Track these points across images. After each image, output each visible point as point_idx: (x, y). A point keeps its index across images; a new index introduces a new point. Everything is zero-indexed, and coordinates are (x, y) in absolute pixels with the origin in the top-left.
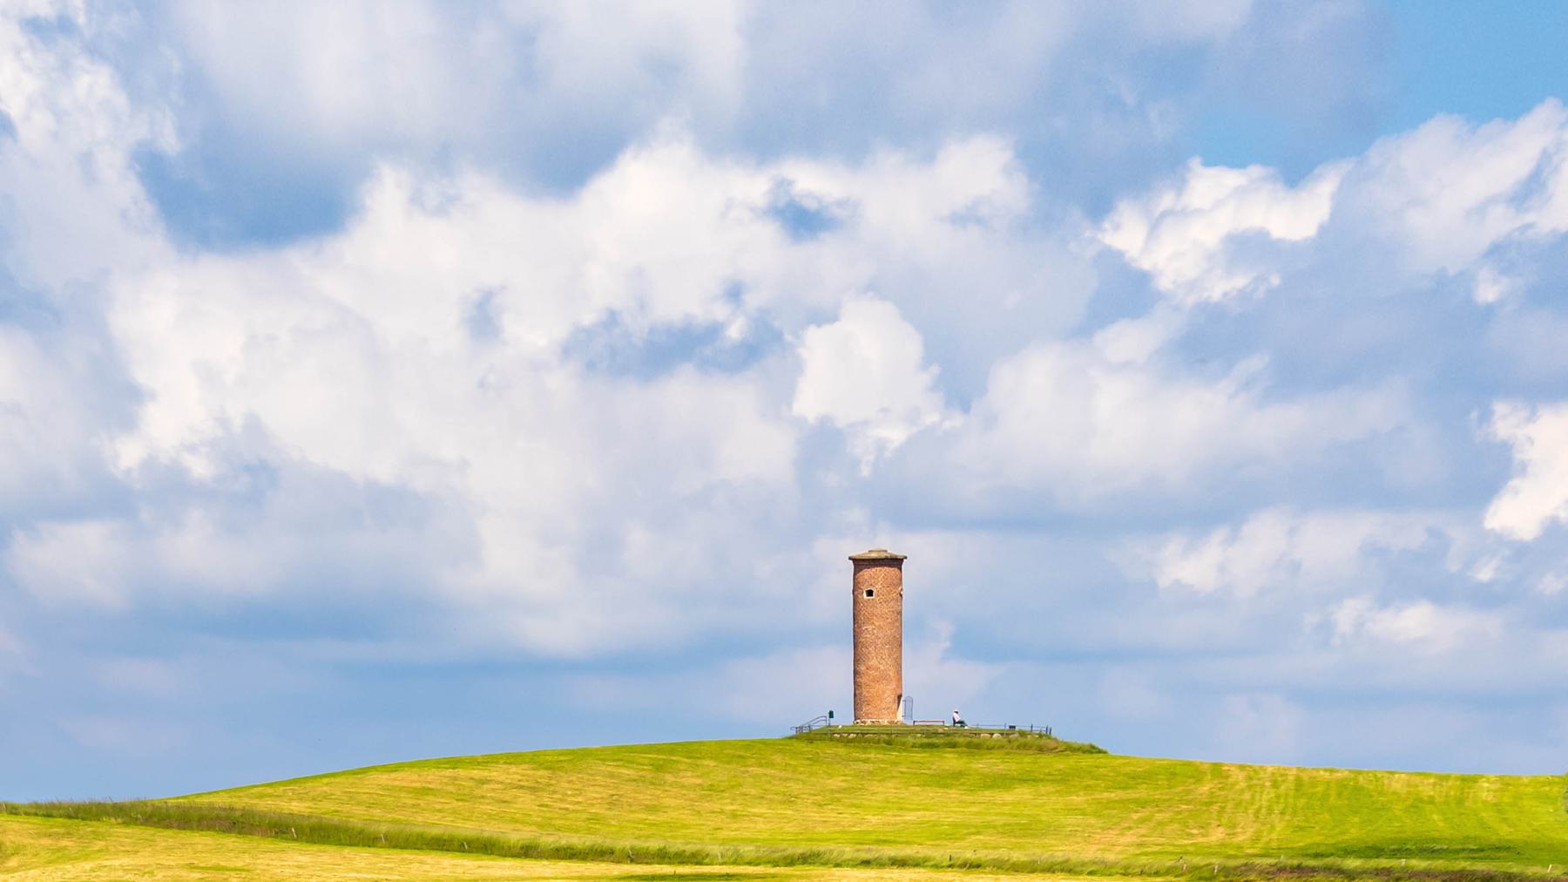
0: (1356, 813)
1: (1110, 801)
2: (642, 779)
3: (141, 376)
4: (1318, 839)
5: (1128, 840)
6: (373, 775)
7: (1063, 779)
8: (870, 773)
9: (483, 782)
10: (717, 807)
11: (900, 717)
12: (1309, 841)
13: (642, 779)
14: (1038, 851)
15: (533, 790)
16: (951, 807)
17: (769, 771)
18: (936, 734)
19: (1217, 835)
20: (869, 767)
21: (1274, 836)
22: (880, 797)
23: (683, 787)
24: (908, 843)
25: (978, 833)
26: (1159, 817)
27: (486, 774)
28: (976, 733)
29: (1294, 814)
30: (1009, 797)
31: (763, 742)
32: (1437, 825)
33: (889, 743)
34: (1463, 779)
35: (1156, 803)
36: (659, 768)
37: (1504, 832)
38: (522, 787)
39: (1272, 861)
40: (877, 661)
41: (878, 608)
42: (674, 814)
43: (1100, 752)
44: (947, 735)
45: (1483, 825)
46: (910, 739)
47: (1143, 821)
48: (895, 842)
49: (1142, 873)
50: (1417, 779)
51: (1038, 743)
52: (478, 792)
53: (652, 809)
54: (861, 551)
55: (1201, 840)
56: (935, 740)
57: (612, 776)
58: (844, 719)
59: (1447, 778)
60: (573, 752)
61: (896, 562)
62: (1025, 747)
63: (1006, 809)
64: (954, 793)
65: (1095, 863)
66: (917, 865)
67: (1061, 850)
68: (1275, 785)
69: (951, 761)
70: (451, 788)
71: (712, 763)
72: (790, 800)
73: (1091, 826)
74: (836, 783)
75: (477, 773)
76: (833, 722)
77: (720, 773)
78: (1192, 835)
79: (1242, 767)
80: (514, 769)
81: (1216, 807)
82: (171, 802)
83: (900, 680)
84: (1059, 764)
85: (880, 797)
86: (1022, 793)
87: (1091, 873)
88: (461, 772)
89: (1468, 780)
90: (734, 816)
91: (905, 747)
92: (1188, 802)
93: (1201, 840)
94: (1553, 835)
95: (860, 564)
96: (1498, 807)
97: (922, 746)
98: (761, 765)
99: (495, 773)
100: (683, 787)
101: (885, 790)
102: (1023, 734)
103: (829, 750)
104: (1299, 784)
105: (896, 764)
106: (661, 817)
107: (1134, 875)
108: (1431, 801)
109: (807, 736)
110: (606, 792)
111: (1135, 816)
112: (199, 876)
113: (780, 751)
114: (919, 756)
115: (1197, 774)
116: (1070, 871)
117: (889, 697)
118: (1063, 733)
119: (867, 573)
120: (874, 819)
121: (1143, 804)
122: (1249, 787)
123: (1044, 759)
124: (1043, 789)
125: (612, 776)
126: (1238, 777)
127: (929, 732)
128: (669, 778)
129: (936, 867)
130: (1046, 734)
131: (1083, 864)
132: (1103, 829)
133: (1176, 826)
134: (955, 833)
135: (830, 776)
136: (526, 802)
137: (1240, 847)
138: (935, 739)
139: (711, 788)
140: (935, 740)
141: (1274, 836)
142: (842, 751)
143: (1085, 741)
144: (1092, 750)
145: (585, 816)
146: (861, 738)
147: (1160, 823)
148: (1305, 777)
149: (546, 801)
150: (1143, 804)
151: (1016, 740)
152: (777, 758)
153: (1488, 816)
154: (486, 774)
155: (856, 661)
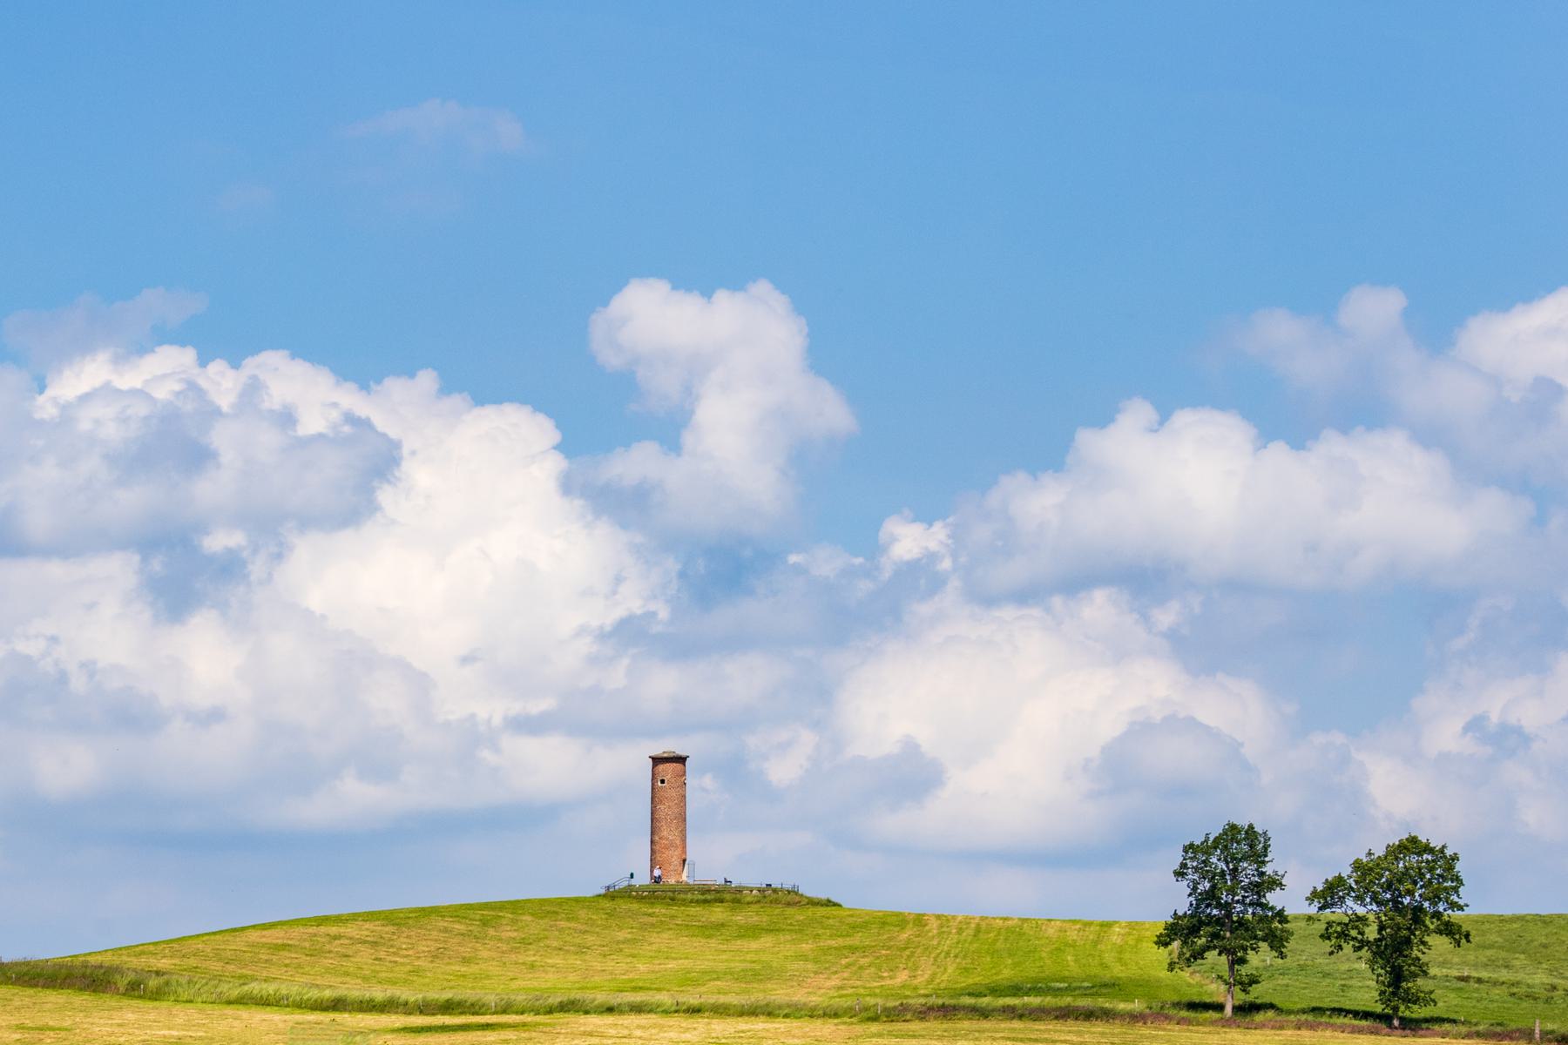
0: (1010, 955)
1: (830, 948)
2: (469, 934)
3: (1184, 418)
4: (977, 979)
5: (830, 983)
6: (248, 933)
7: (800, 930)
8: (653, 925)
9: (336, 938)
10: (521, 959)
11: (684, 877)
12: (970, 981)
13: (469, 934)
14: (761, 996)
15: (375, 944)
16: (706, 955)
17: (573, 925)
18: (709, 891)
19: (902, 977)
20: (653, 920)
21: (945, 977)
22: (654, 947)
23: (500, 940)
24: (658, 990)
25: (718, 979)
26: (863, 961)
27: (342, 930)
28: (739, 890)
29: (965, 957)
30: (754, 945)
31: (577, 900)
32: (1071, 965)
33: (673, 899)
34: (1102, 925)
35: (864, 949)
36: (485, 923)
37: (1118, 971)
38: (365, 942)
39: (922, 1001)
40: (668, 833)
41: (669, 792)
42: (483, 966)
43: (835, 905)
44: (717, 891)
45: (1105, 966)
46: (689, 896)
47: (847, 966)
48: (649, 989)
49: (825, 1015)
50: (1067, 925)
51: (790, 898)
52: (328, 947)
53: (466, 961)
54: (658, 751)
55: (888, 982)
56: (708, 897)
57: (446, 930)
58: (643, 879)
59: (1090, 924)
60: (423, 909)
61: (681, 760)
62: (777, 901)
63: (748, 957)
64: (713, 943)
65: (789, 1006)
66: (650, 1011)
67: (779, 994)
68: (960, 931)
69: (718, 913)
70: (307, 944)
71: (529, 918)
72: (582, 950)
73: (806, 971)
74: (621, 935)
75: (334, 930)
76: (633, 882)
77: (533, 926)
78: (882, 978)
79: (938, 917)
80: (367, 925)
81: (907, 952)
82: (93, 960)
83: (684, 847)
84: (797, 915)
85: (654, 947)
86: (766, 941)
87: (786, 1016)
88: (323, 929)
89: (1106, 926)
90: (532, 966)
91: (684, 903)
92: (889, 948)
93: (888, 982)
94: (1153, 973)
95: (657, 761)
96: (1120, 950)
97: (697, 901)
98: (568, 919)
99: (351, 930)
100: (500, 940)
101: (660, 940)
102: (775, 891)
103: (624, 905)
104: (978, 930)
105: (673, 917)
106: (474, 969)
107: (819, 1016)
108: (1073, 945)
109: (612, 894)
110: (434, 946)
111: (844, 961)
112: (17, 1036)
113: (589, 908)
114: (694, 910)
115: (901, 921)
116: (770, 1014)
117: (676, 861)
118: (808, 891)
119: (661, 767)
120: (641, 967)
121: (853, 949)
122: (940, 934)
123: (790, 911)
124: (781, 937)
125: (446, 930)
126: (934, 924)
127: (705, 890)
128: (491, 932)
129: (666, 1012)
130: (793, 891)
131: (780, 1007)
132: (816, 973)
133: (873, 969)
134: (688, 980)
135: (620, 928)
136: (365, 956)
137: (915, 988)
138: (713, 895)
139: (523, 941)
140: (708, 897)
141: (945, 977)
142: (635, 906)
143: (823, 896)
144: (829, 903)
145: (409, 968)
146: (659, 893)
147: (861, 968)
148: (983, 925)
149: (382, 955)
150: (853, 949)
151: (771, 896)
152: (582, 914)
153: (1109, 957)
154: (342, 930)
155: (652, 833)
